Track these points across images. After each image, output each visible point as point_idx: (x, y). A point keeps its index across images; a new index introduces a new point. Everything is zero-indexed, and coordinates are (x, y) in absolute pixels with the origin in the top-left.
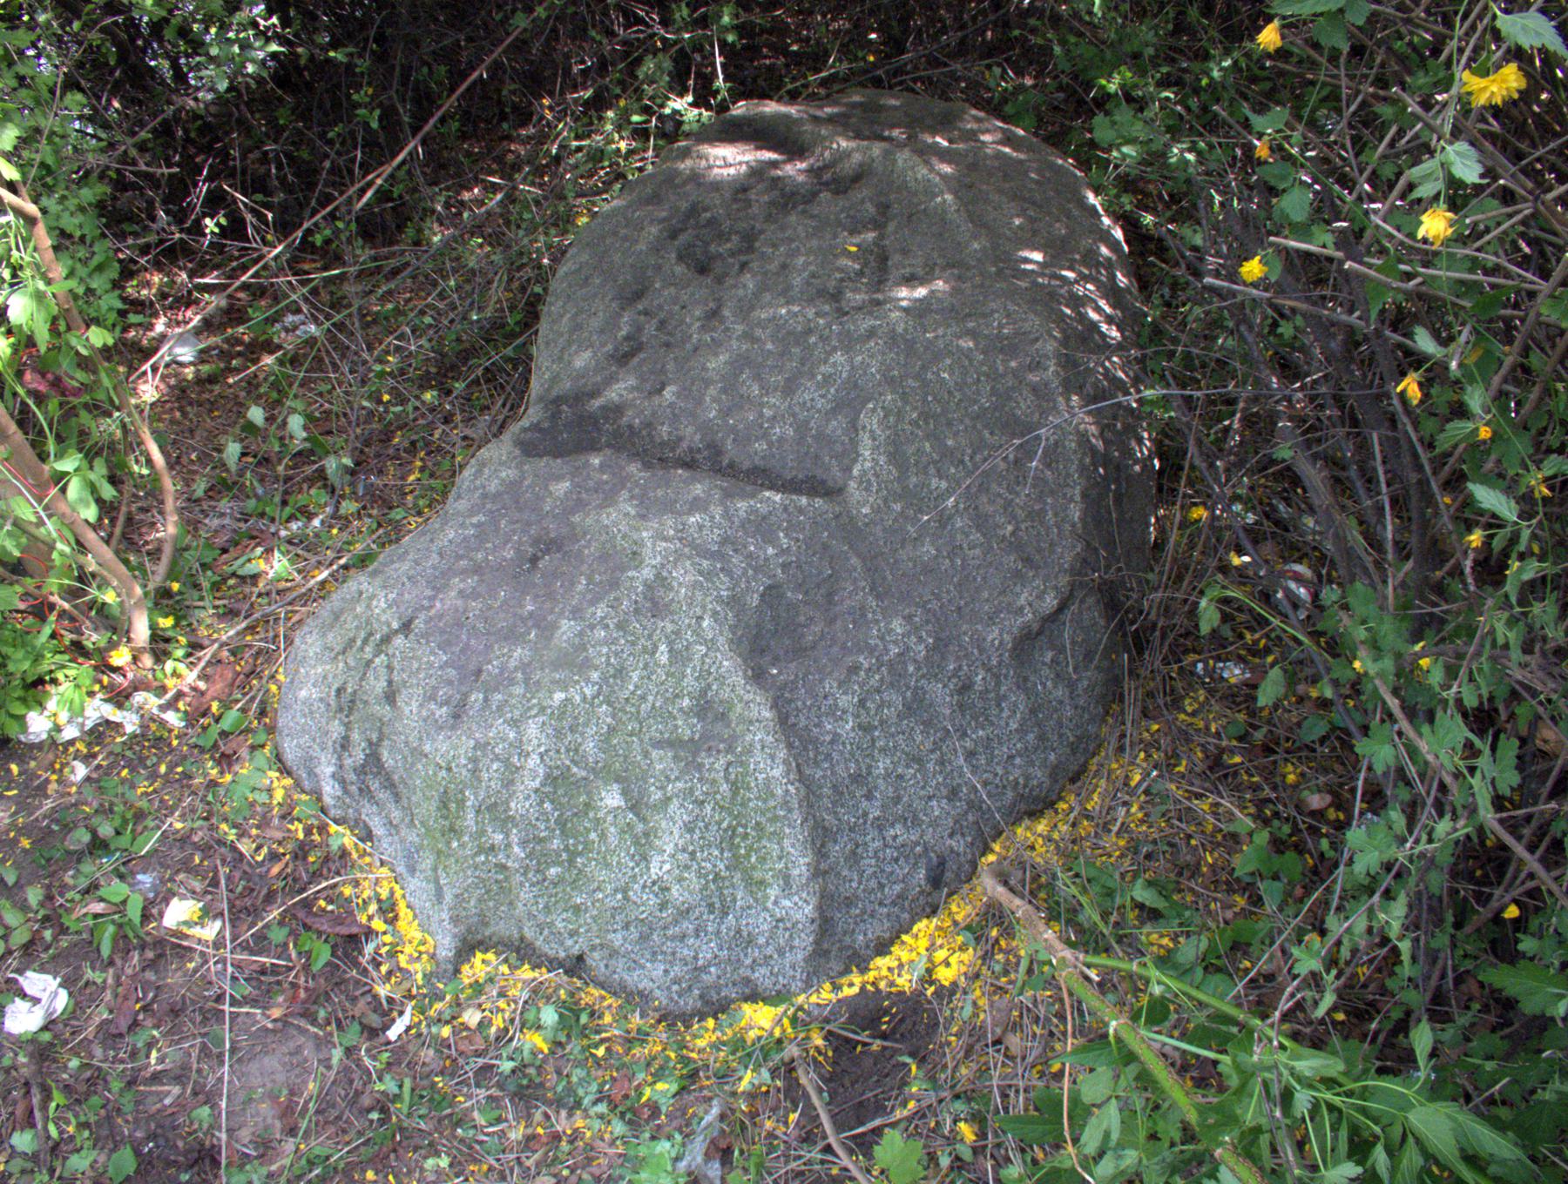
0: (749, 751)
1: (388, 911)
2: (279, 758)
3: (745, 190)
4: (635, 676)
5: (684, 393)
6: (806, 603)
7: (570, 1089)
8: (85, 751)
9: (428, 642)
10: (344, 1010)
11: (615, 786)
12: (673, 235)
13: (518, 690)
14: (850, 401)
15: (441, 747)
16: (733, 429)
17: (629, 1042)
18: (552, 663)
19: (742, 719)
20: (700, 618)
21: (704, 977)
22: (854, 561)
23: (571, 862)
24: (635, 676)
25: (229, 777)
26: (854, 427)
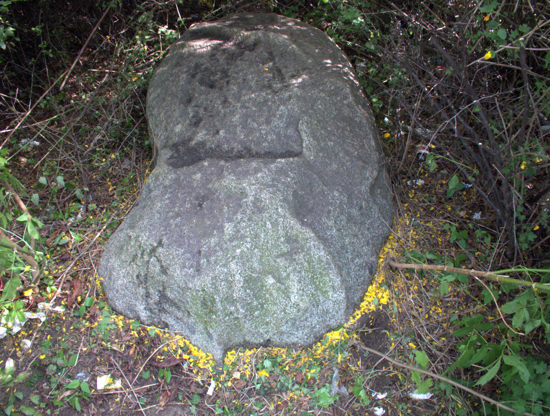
0: (309, 249)
1: (186, 350)
2: (113, 310)
3: (213, 55)
4: (262, 235)
5: (228, 132)
6: (305, 194)
7: (282, 385)
8: (26, 334)
9: (172, 247)
10: (188, 392)
11: (270, 276)
12: (193, 76)
13: (220, 253)
14: (293, 122)
15: (197, 283)
16: (252, 141)
17: (295, 361)
18: (229, 240)
19: (303, 239)
20: (277, 209)
21: (315, 330)
22: (315, 176)
23: (262, 307)
24: (262, 235)
25: (96, 324)
26: (297, 130)
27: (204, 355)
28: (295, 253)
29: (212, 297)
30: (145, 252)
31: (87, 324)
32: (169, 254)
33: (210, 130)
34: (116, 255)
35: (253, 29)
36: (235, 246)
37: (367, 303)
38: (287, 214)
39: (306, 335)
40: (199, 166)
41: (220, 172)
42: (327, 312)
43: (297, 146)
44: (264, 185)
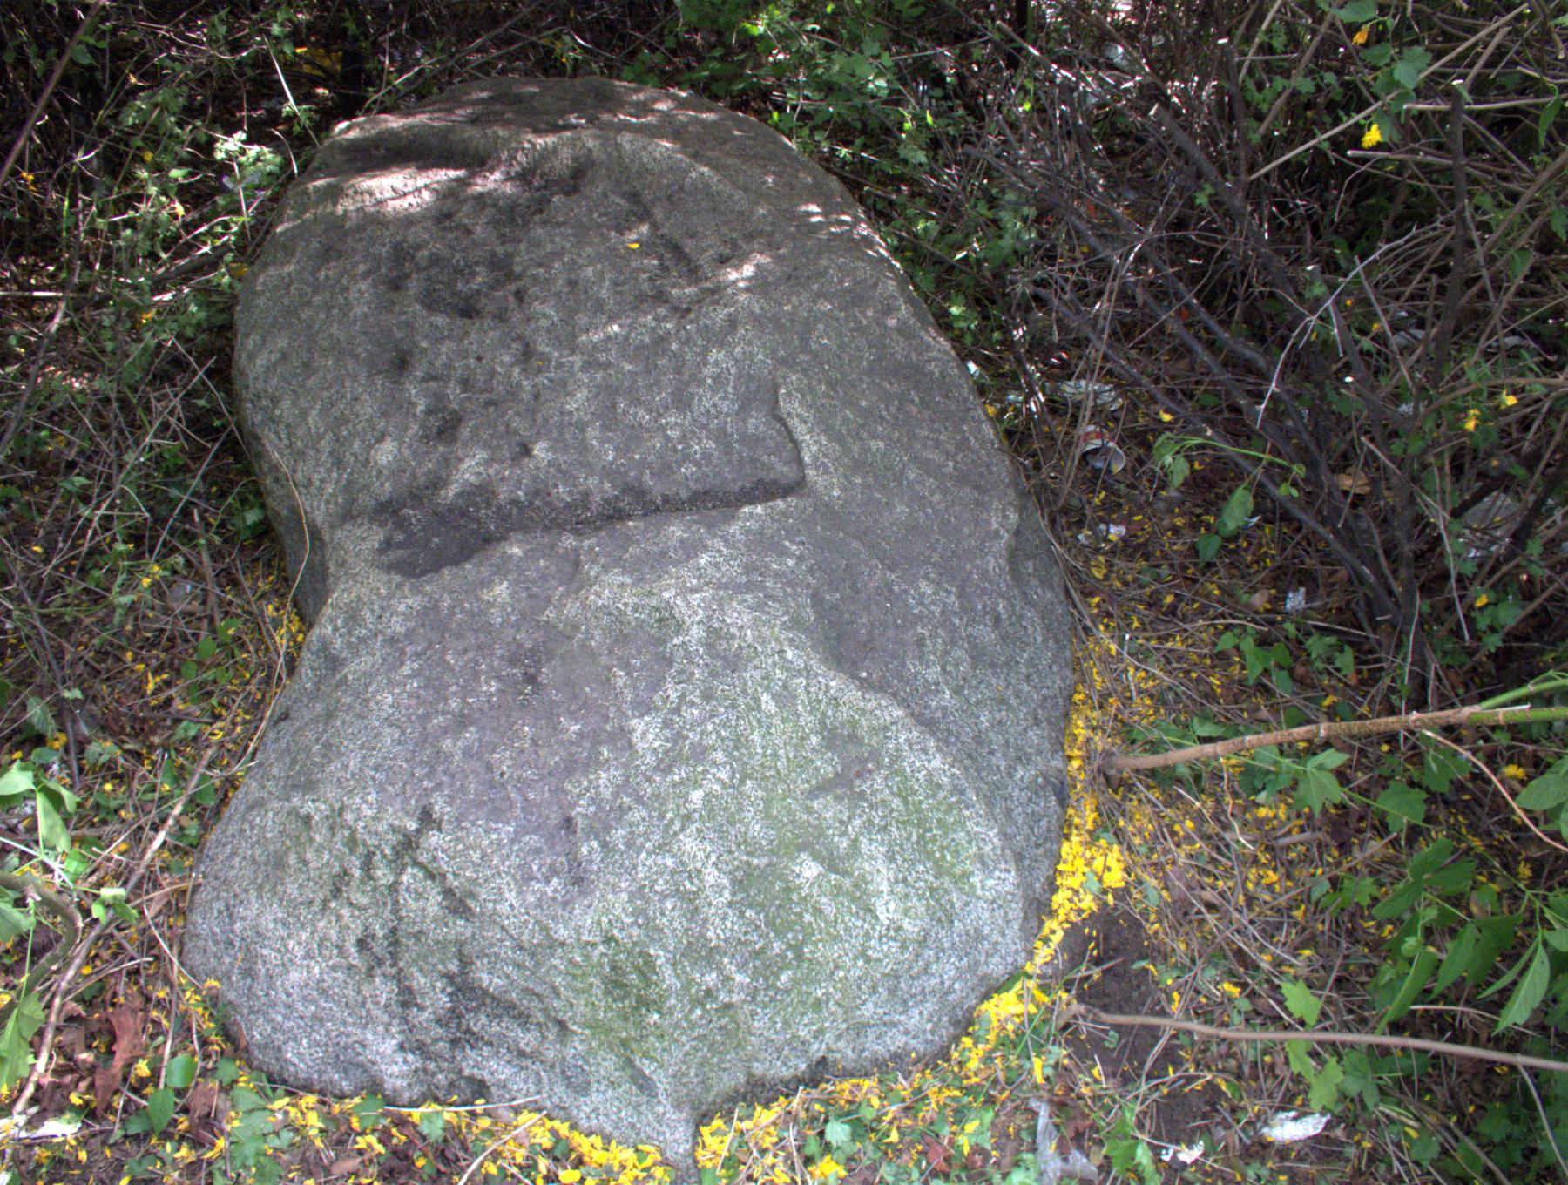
0: (897, 756)
4: (756, 737)
5: (558, 445)
9: (473, 823)
12: (396, 285)
15: (584, 920)
16: (643, 464)
18: (656, 768)
19: (874, 730)
20: (781, 651)
22: (855, 544)
23: (799, 956)
25: (221, 1143)
27: (629, 1155)
28: (859, 775)
29: (640, 954)
30: (378, 857)
31: (184, 1151)
32: (467, 848)
33: (499, 447)
34: (261, 887)
35: (555, 129)
36: (682, 783)
37: (1069, 894)
38: (814, 664)
39: (929, 1021)
40: (496, 560)
41: (568, 568)
42: (978, 936)
43: (786, 464)
44: (726, 587)
